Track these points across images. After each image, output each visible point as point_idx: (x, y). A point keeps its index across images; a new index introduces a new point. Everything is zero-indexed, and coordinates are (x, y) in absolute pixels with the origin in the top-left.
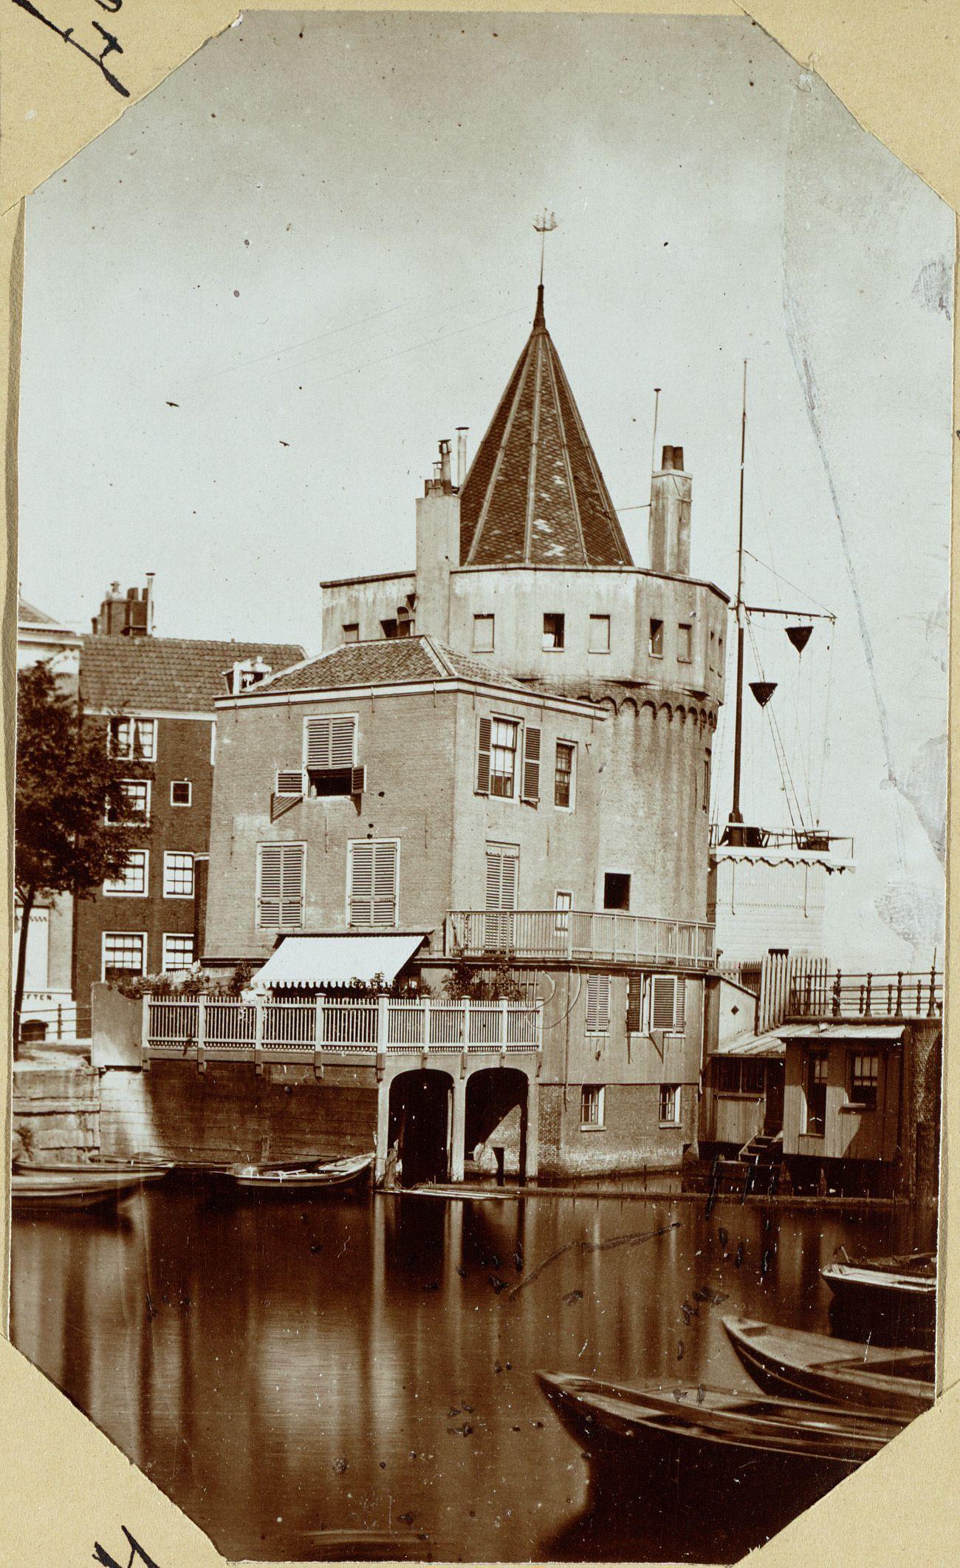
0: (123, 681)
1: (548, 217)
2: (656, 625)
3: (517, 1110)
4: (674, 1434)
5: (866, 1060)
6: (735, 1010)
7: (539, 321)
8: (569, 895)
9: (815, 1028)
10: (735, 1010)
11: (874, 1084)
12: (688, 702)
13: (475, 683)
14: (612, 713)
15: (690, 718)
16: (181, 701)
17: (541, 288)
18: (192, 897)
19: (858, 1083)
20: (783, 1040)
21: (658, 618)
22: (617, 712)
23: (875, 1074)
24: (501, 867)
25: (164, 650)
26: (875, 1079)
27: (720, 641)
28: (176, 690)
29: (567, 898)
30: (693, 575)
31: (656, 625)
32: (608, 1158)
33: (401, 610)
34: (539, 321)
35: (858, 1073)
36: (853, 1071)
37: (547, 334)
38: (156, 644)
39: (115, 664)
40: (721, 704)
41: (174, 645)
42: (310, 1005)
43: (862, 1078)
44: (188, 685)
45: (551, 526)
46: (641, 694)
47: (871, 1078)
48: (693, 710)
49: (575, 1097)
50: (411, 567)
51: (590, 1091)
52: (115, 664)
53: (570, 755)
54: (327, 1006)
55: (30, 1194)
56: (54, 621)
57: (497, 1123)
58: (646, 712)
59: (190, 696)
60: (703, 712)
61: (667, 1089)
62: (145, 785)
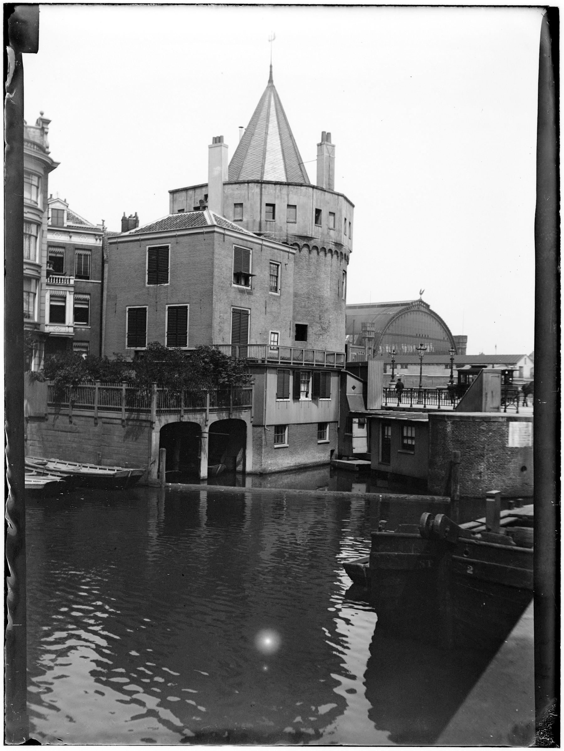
2: (318, 212)
5: (410, 428)
7: (271, 81)
8: (277, 334)
12: (334, 248)
13: (225, 229)
14: (298, 250)
15: (335, 256)
17: (271, 66)
19: (405, 442)
23: (414, 435)
24: (240, 319)
27: (350, 223)
29: (276, 336)
30: (336, 190)
31: (318, 212)
32: (287, 461)
33: (201, 201)
34: (271, 81)
35: (405, 434)
37: (274, 87)
40: (351, 252)
43: (407, 438)
46: (312, 243)
47: (412, 438)
49: (271, 432)
50: (205, 181)
56: (84, 224)
57: (200, 460)
60: (341, 253)
61: (322, 426)
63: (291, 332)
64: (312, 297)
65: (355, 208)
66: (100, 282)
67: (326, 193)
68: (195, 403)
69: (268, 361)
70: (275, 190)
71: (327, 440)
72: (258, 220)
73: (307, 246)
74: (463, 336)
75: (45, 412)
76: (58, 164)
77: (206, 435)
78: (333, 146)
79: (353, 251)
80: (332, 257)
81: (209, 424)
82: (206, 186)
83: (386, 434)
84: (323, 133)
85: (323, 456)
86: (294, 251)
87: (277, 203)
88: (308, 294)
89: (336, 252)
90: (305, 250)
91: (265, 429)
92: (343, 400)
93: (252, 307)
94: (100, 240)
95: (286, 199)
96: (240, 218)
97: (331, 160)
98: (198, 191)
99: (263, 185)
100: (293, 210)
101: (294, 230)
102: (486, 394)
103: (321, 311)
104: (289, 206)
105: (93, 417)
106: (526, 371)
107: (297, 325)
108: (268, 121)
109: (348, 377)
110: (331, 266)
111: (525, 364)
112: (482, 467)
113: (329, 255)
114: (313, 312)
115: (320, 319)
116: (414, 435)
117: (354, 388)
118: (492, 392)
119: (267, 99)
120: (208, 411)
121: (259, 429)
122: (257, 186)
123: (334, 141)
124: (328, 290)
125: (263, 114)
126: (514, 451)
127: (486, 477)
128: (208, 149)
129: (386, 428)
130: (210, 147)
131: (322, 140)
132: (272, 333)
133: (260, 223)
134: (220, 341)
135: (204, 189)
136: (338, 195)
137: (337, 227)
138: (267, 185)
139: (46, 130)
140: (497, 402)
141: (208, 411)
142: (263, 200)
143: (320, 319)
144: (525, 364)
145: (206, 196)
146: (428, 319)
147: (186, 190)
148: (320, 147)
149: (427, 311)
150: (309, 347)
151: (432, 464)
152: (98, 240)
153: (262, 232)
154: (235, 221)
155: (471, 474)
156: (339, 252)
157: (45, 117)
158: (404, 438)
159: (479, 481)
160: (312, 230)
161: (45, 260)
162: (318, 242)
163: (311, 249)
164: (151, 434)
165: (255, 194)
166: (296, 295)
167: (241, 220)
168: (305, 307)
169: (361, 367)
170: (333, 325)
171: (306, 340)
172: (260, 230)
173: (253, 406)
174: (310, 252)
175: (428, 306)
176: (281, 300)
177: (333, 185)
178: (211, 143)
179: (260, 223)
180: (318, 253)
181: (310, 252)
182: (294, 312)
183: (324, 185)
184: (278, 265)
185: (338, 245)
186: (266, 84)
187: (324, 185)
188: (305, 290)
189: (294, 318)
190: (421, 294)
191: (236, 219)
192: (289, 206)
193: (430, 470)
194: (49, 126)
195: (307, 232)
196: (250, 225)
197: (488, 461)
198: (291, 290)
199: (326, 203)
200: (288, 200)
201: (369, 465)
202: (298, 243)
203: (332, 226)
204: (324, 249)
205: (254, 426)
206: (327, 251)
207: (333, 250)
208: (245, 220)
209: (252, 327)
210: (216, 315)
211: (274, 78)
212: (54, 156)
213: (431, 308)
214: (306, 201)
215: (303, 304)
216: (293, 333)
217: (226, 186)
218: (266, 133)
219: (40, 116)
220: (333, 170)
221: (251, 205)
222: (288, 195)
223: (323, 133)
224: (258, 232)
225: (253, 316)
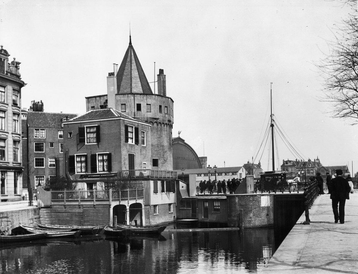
3: (139, 213)
4: (185, 221)
7: (130, 43)
8: (146, 164)
11: (219, 208)
17: (130, 36)
19: (215, 208)
22: (153, 125)
25: (46, 115)
26: (219, 206)
29: (145, 165)
30: (167, 96)
31: (160, 106)
34: (130, 43)
35: (215, 205)
36: (214, 204)
37: (172, 126)
38: (44, 114)
43: (216, 206)
47: (218, 206)
48: (168, 124)
49: (152, 208)
50: (106, 94)
51: (155, 206)
53: (144, 133)
55: (55, 236)
60: (170, 125)
61: (170, 204)
63: (151, 163)
64: (159, 146)
66: (27, 138)
67: (163, 98)
68: (124, 196)
69: (151, 177)
70: (141, 97)
71: (172, 212)
72: (133, 111)
73: (156, 122)
74: (204, 157)
75: (50, 205)
76: (26, 84)
77: (128, 210)
78: (165, 76)
80: (164, 126)
81: (129, 205)
82: (106, 95)
83: (205, 205)
85: (172, 219)
86: (150, 125)
87: (142, 103)
88: (158, 145)
89: (168, 124)
90: (155, 125)
91: (150, 207)
92: (178, 195)
93: (136, 152)
94: (26, 116)
95: (146, 101)
96: (125, 111)
97: (164, 82)
98: (102, 98)
99: (135, 95)
101: (150, 115)
102: (248, 186)
103: (163, 152)
104: (147, 104)
105: (63, 205)
107: (153, 159)
108: (131, 63)
109: (180, 182)
111: (243, 172)
112: (251, 215)
113: (166, 126)
114: (160, 153)
115: (163, 156)
116: (219, 205)
117: (183, 187)
118: (250, 185)
119: (130, 52)
120: (129, 199)
121: (148, 207)
122: (132, 96)
123: (165, 73)
124: (166, 142)
125: (128, 60)
126: (264, 208)
127: (253, 219)
128: (106, 78)
129: (205, 203)
130: (107, 78)
131: (160, 73)
132: (144, 164)
133: (134, 113)
134: (125, 169)
135: (105, 97)
136: (168, 98)
137: (168, 113)
138: (137, 95)
139: (18, 68)
140: (253, 189)
141: (129, 199)
142: (135, 102)
143: (163, 156)
144: (243, 172)
145: (107, 101)
146: (184, 148)
147: (95, 97)
148: (159, 76)
150: (159, 169)
151: (230, 216)
152: (25, 116)
153: (135, 117)
154: (122, 112)
155: (247, 218)
156: (170, 124)
157: (17, 60)
158: (214, 206)
159: (251, 221)
160: (159, 116)
161: (21, 132)
164: (110, 210)
165: (131, 99)
166: (152, 145)
167: (125, 112)
168: (156, 151)
169: (184, 177)
170: (169, 158)
171: (157, 166)
172: (135, 116)
173: (144, 197)
175: (183, 141)
176: (147, 148)
177: (166, 93)
178: (108, 76)
179: (134, 113)
180: (161, 125)
181: (157, 125)
182: (152, 154)
183: (162, 94)
184: (144, 132)
185: (169, 121)
186: (128, 45)
187: (162, 94)
188: (156, 143)
189: (152, 156)
191: (122, 111)
192: (147, 104)
193: (229, 218)
194: (20, 65)
196: (130, 114)
197: (254, 212)
198: (150, 143)
200: (147, 102)
201: (198, 221)
203: (166, 112)
205: (145, 206)
207: (167, 123)
208: (127, 111)
209: (136, 161)
210: (123, 157)
211: (132, 42)
212: (23, 79)
213: (186, 142)
215: (156, 150)
216: (152, 163)
217: (117, 96)
218: (131, 69)
219: (13, 60)
220: (165, 87)
221: (130, 104)
222: (147, 100)
224: (134, 117)
225: (136, 156)
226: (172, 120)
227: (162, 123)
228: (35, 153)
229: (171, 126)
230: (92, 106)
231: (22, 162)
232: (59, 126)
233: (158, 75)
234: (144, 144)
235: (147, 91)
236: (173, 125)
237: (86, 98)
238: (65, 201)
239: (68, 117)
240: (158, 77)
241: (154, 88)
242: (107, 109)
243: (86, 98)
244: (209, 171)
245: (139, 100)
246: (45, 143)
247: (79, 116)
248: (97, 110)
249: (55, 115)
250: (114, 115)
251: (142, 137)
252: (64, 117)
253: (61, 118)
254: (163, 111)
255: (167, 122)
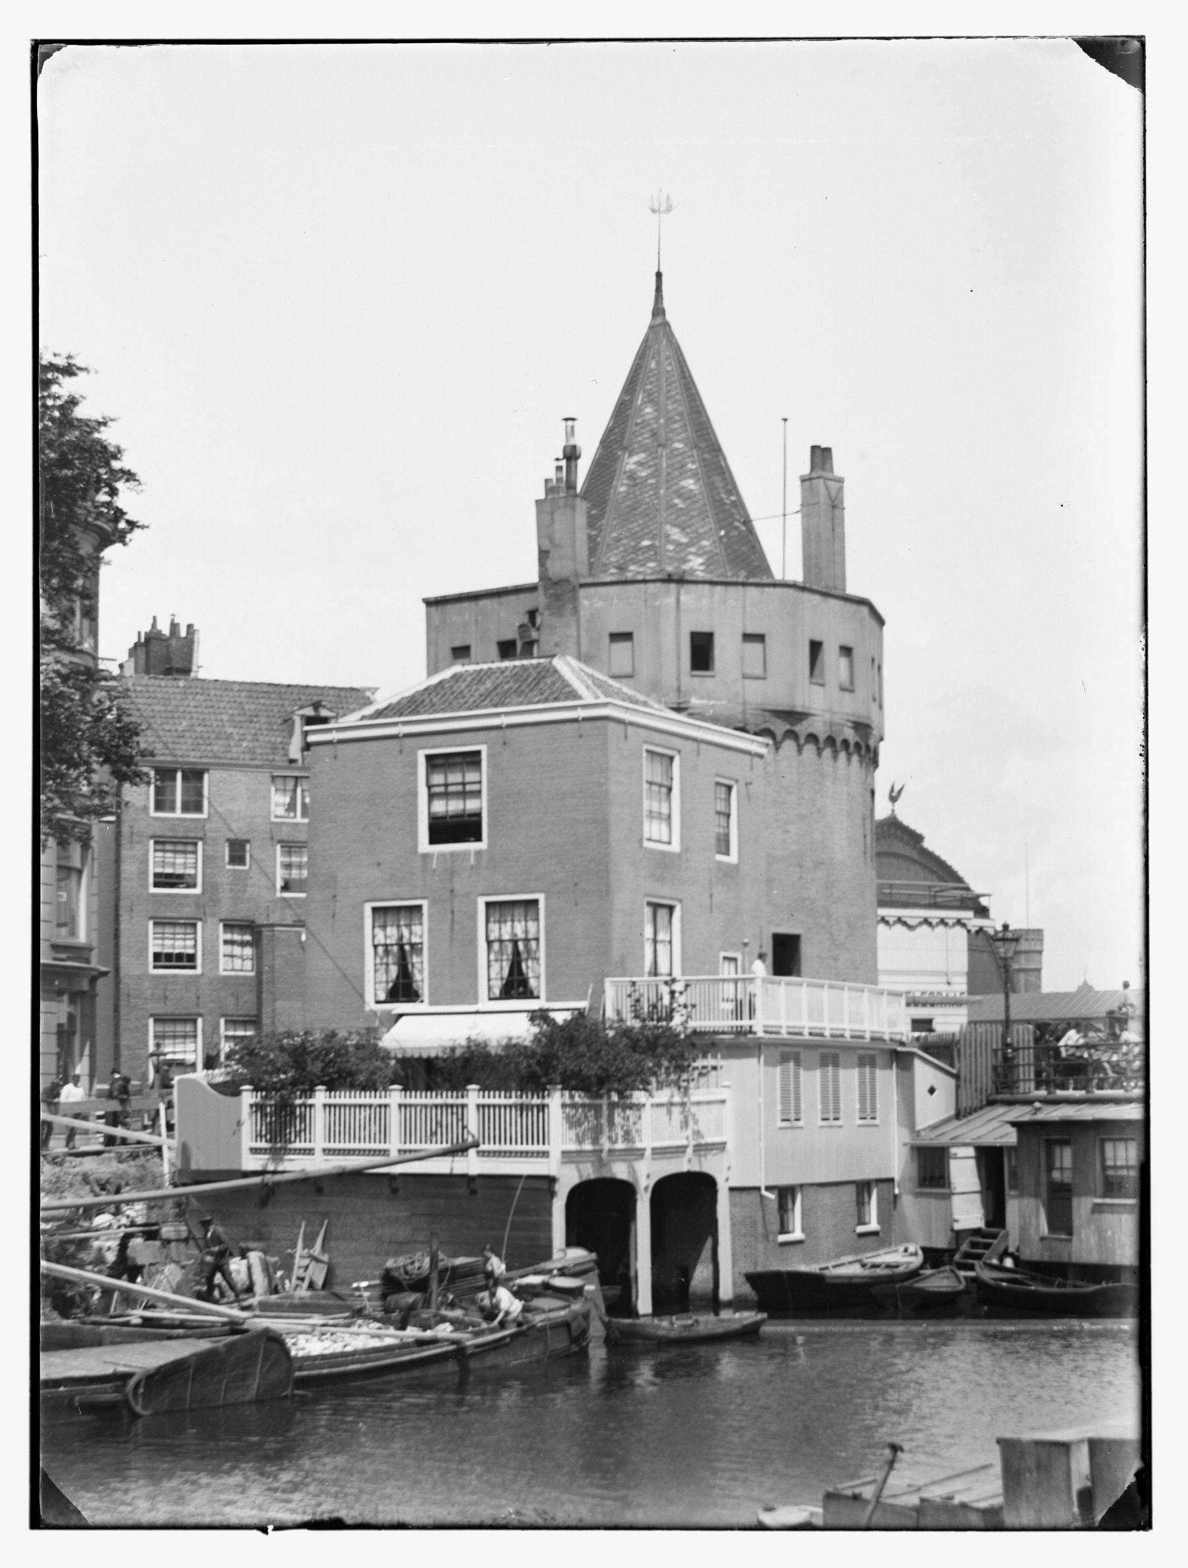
0: (167, 727)
1: (663, 200)
2: (816, 647)
6: (932, 1091)
8: (735, 960)
9: (1027, 1109)
10: (932, 1091)
12: (850, 734)
14: (772, 748)
16: (234, 750)
17: (659, 275)
18: (252, 974)
20: (1014, 1124)
21: (817, 638)
28: (229, 737)
30: (852, 589)
31: (816, 647)
35: (1110, 1163)
39: (157, 708)
41: (225, 686)
42: (460, 1101)
43: (1115, 1167)
44: (242, 731)
45: (687, 534)
52: (157, 708)
54: (482, 1101)
58: (810, 749)
59: (245, 744)
62: (276, 817)
65: (885, 628)
70: (712, 596)
73: (792, 735)
78: (840, 481)
79: (886, 737)
84: (815, 449)
97: (835, 505)
100: (756, 647)
106: (871, 1441)
109: (918, 1063)
110: (848, 780)
123: (840, 466)
131: (813, 468)
132: (725, 958)
145: (532, 614)
148: (807, 483)
149: (915, 855)
162: (818, 726)
163: (779, 738)
174: (800, 750)
175: (917, 838)
184: (729, 788)
185: (863, 728)
186: (645, 319)
190: (893, 799)
195: (500, 604)
199: (833, 624)
202: (772, 728)
204: (831, 740)
206: (838, 744)
211: (667, 304)
213: (927, 844)
214: (794, 623)
223: (815, 449)
226: (874, 724)
227: (822, 737)
228: (154, 895)
229: (870, 758)
230: (458, 644)
231: (95, 944)
232: (274, 749)
233: (803, 480)
234: (727, 853)
235: (743, 559)
236: (883, 748)
237: (429, 603)
238: (318, 1152)
239: (324, 707)
240: (803, 491)
241: (785, 557)
242: (534, 661)
243: (429, 603)
244: (1005, 959)
245: (701, 608)
246: (205, 844)
247: (382, 700)
248: (485, 666)
249: (255, 690)
250: (574, 695)
251: (719, 813)
252: (302, 707)
253: (289, 709)
254: (829, 675)
255: (850, 734)
